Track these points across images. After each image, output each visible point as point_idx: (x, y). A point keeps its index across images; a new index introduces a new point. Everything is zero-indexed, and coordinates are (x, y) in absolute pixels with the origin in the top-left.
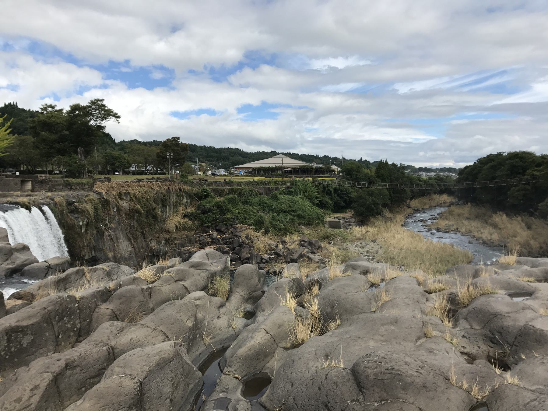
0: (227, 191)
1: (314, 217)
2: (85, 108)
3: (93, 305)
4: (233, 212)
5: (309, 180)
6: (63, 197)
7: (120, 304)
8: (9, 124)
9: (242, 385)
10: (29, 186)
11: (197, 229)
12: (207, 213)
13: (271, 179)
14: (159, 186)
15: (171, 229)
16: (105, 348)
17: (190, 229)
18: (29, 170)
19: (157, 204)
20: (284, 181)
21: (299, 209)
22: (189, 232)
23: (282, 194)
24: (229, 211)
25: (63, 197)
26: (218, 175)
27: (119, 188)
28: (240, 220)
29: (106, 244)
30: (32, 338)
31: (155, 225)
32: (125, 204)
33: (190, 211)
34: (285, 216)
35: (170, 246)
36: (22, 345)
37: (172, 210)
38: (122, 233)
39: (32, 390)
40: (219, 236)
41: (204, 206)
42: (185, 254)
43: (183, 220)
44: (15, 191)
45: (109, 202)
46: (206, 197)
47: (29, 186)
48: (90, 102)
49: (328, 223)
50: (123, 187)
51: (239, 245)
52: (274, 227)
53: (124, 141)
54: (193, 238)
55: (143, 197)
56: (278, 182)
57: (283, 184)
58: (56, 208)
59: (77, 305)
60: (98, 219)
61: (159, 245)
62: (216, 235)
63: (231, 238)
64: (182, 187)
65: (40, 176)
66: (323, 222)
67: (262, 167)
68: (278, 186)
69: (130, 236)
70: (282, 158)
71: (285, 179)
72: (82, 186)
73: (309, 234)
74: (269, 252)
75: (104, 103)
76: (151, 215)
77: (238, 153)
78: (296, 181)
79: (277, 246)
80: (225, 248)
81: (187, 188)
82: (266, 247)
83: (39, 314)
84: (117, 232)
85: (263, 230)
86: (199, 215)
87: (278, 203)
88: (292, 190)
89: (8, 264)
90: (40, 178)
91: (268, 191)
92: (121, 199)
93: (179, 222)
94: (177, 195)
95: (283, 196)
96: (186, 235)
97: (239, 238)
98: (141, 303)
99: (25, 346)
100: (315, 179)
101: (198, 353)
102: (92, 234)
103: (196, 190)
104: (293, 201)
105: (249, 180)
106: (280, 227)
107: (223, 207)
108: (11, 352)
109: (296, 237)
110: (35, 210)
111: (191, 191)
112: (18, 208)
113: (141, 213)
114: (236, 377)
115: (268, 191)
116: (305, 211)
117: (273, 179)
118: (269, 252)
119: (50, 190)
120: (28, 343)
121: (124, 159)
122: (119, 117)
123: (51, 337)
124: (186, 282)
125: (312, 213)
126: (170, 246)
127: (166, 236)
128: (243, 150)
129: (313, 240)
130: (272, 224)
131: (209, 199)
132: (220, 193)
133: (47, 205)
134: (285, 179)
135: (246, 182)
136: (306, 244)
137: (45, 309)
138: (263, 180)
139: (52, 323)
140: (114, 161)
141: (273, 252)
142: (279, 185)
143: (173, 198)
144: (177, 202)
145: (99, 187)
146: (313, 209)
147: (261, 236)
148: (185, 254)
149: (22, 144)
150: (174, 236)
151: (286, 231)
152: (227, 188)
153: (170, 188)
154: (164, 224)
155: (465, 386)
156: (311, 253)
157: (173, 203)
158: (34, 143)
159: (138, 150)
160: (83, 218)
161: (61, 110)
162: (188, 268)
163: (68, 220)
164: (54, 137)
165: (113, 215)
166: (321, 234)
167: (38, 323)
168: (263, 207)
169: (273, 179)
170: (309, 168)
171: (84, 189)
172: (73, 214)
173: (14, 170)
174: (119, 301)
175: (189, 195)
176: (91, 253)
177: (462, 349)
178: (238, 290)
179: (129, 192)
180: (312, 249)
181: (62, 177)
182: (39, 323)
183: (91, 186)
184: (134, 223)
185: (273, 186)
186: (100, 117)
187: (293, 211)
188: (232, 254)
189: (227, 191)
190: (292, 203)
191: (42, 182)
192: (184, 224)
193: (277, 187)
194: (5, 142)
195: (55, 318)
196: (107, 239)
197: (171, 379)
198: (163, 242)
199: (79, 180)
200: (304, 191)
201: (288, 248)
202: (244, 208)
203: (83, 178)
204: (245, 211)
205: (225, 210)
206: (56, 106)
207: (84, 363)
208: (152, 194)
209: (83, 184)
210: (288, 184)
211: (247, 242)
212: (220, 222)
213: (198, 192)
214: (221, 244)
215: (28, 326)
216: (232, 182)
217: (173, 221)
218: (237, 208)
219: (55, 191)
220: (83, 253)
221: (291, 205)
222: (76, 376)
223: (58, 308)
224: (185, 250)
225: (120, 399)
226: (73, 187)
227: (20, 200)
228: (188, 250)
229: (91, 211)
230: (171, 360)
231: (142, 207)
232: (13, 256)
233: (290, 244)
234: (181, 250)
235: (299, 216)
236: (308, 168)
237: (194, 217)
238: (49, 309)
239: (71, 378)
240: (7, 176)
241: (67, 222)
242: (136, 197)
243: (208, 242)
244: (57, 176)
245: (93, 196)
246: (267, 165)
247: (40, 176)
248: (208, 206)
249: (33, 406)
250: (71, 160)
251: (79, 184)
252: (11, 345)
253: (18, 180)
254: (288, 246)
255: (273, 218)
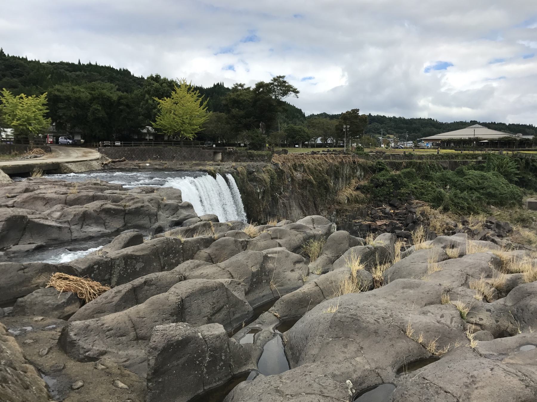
0: (405, 164)
1: (508, 196)
2: (268, 85)
3: (196, 249)
4: (409, 187)
5: (508, 153)
6: (245, 167)
7: (216, 250)
8: (206, 103)
9: (279, 322)
10: (219, 157)
11: (370, 202)
12: (380, 187)
13: (460, 152)
14: (333, 159)
15: (342, 201)
16: (178, 276)
17: (362, 202)
18: (223, 143)
19: (331, 176)
20: (475, 155)
21: (489, 187)
22: (360, 205)
23: (471, 169)
24: (404, 186)
25: (245, 167)
26: (402, 148)
27: (294, 160)
28: (416, 195)
29: (280, 211)
30: (143, 265)
31: (326, 196)
32: (299, 175)
33: (363, 184)
34: (471, 193)
35: (340, 217)
36: (136, 269)
37: (345, 182)
38: (295, 202)
39: (116, 293)
40: (392, 211)
41: (377, 179)
42: (355, 226)
43: (355, 193)
44: (208, 161)
45: (284, 172)
46: (381, 170)
47: (219, 157)
48: (272, 79)
49: (527, 204)
50: (298, 158)
51: (413, 221)
52: (456, 205)
53: (313, 114)
54: (365, 211)
55: (316, 169)
56: (468, 155)
57: (473, 158)
58: (238, 176)
59: (181, 246)
60: (274, 188)
61: (330, 215)
62: (388, 209)
63: (405, 214)
64: (356, 160)
65: (229, 148)
66: (521, 204)
67: (452, 139)
68: (467, 160)
69: (302, 205)
70: (474, 129)
71: (477, 152)
72: (262, 158)
73: (500, 215)
74: (446, 231)
75: (285, 79)
76: (323, 185)
77: (431, 124)
78: (489, 154)
79: (456, 226)
80: (398, 224)
81: (361, 160)
82: (443, 226)
83: (149, 249)
84: (291, 201)
85: (441, 208)
86: (372, 188)
87: (464, 179)
88: (484, 165)
89: (175, 217)
90: (228, 150)
91: (454, 166)
92: (296, 170)
93: (351, 194)
94: (351, 168)
95: (471, 172)
96: (358, 208)
97: (413, 215)
98: (232, 251)
99: (138, 269)
100: (515, 152)
101: (261, 295)
102: (268, 201)
103: (370, 162)
104: (483, 177)
105: (433, 153)
106: (463, 205)
107: (398, 181)
108: (128, 273)
109: (482, 218)
110: (219, 177)
111: (365, 164)
112: (205, 175)
113: (313, 184)
114: (275, 315)
115: (454, 166)
116: (496, 189)
117: (462, 153)
118: (446, 231)
119: (236, 161)
120: (140, 268)
121: (304, 132)
122: (298, 92)
123: (157, 266)
124: (282, 240)
125: (506, 192)
126: (340, 217)
127: (337, 207)
128: (436, 121)
129: (502, 223)
130: (453, 202)
131: (383, 172)
132: (397, 166)
133: (231, 174)
134: (477, 152)
135: (429, 155)
136: (493, 226)
137: (155, 245)
138: (449, 153)
139: (159, 256)
140: (295, 134)
141: (451, 231)
142: (469, 159)
143: (347, 171)
144: (350, 174)
145: (277, 159)
146: (509, 187)
147: (439, 214)
148: (355, 226)
149: (219, 119)
150: (345, 208)
151: (471, 210)
152: (405, 161)
153: (344, 161)
154: (336, 196)
155: (421, 340)
156: (498, 236)
157: (346, 175)
158: (226, 119)
159: (318, 124)
160: (260, 186)
161: (249, 88)
162: (288, 229)
163: (248, 187)
164: (242, 113)
165: (287, 185)
166: (516, 216)
167: (148, 255)
168: (444, 182)
169: (462, 153)
170: (511, 140)
171: (263, 161)
172: (252, 183)
173: (212, 143)
174: (215, 248)
175: (364, 168)
176: (267, 218)
177: (478, 320)
178: (327, 252)
179: (303, 164)
180: (499, 232)
181: (246, 150)
182: (149, 255)
183: (270, 157)
184: (306, 193)
185: (461, 160)
186: (281, 93)
187: (482, 189)
188: (404, 230)
189: (405, 164)
190: (481, 179)
191: (230, 153)
192: (356, 197)
193: (466, 161)
194: (203, 118)
195: (162, 253)
196: (281, 206)
197: (212, 304)
198: (334, 213)
199: (260, 152)
200: (500, 167)
201: (470, 229)
202: (422, 183)
203: (263, 150)
204: (422, 186)
205: (400, 184)
206: (244, 84)
207: (159, 283)
208: (325, 167)
209: (262, 156)
210: (480, 158)
211: (422, 219)
212: (394, 197)
213: (372, 165)
214: (394, 219)
215: (140, 255)
216: (412, 155)
217: (345, 193)
218: (414, 182)
219: (240, 161)
220: (259, 217)
221: (480, 181)
222: (152, 291)
223: (165, 246)
224: (356, 223)
225: (165, 307)
226: (255, 158)
227: (208, 168)
228: (358, 222)
229: (268, 180)
230: (214, 289)
231: (314, 178)
232: (179, 212)
233: (473, 224)
234: (352, 222)
235: (490, 195)
236: (510, 140)
237: (367, 190)
238: (157, 246)
239: (148, 291)
240: (203, 148)
241: (247, 189)
242: (309, 169)
243: (380, 216)
244: (242, 148)
245: (270, 167)
246: (458, 137)
247: (229, 148)
248: (382, 179)
249: (114, 303)
250: (254, 133)
251: (259, 156)
252: (128, 267)
253: (211, 152)
254: (470, 226)
255: (456, 195)
